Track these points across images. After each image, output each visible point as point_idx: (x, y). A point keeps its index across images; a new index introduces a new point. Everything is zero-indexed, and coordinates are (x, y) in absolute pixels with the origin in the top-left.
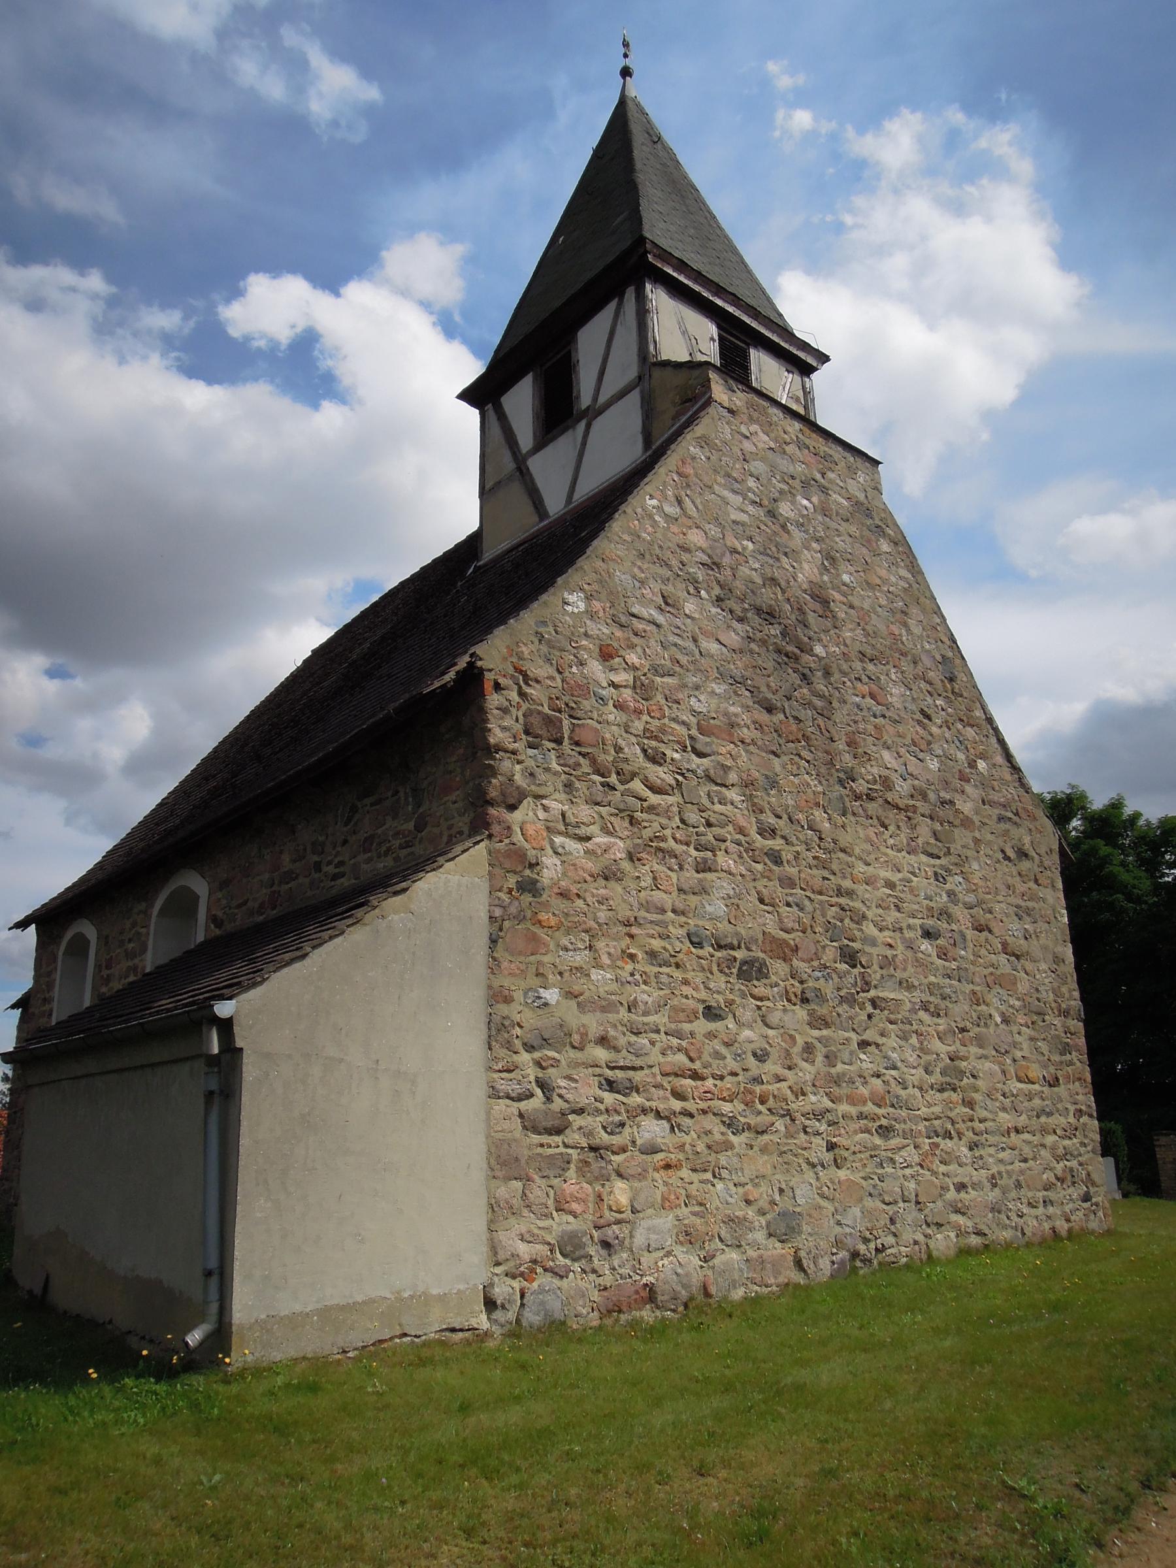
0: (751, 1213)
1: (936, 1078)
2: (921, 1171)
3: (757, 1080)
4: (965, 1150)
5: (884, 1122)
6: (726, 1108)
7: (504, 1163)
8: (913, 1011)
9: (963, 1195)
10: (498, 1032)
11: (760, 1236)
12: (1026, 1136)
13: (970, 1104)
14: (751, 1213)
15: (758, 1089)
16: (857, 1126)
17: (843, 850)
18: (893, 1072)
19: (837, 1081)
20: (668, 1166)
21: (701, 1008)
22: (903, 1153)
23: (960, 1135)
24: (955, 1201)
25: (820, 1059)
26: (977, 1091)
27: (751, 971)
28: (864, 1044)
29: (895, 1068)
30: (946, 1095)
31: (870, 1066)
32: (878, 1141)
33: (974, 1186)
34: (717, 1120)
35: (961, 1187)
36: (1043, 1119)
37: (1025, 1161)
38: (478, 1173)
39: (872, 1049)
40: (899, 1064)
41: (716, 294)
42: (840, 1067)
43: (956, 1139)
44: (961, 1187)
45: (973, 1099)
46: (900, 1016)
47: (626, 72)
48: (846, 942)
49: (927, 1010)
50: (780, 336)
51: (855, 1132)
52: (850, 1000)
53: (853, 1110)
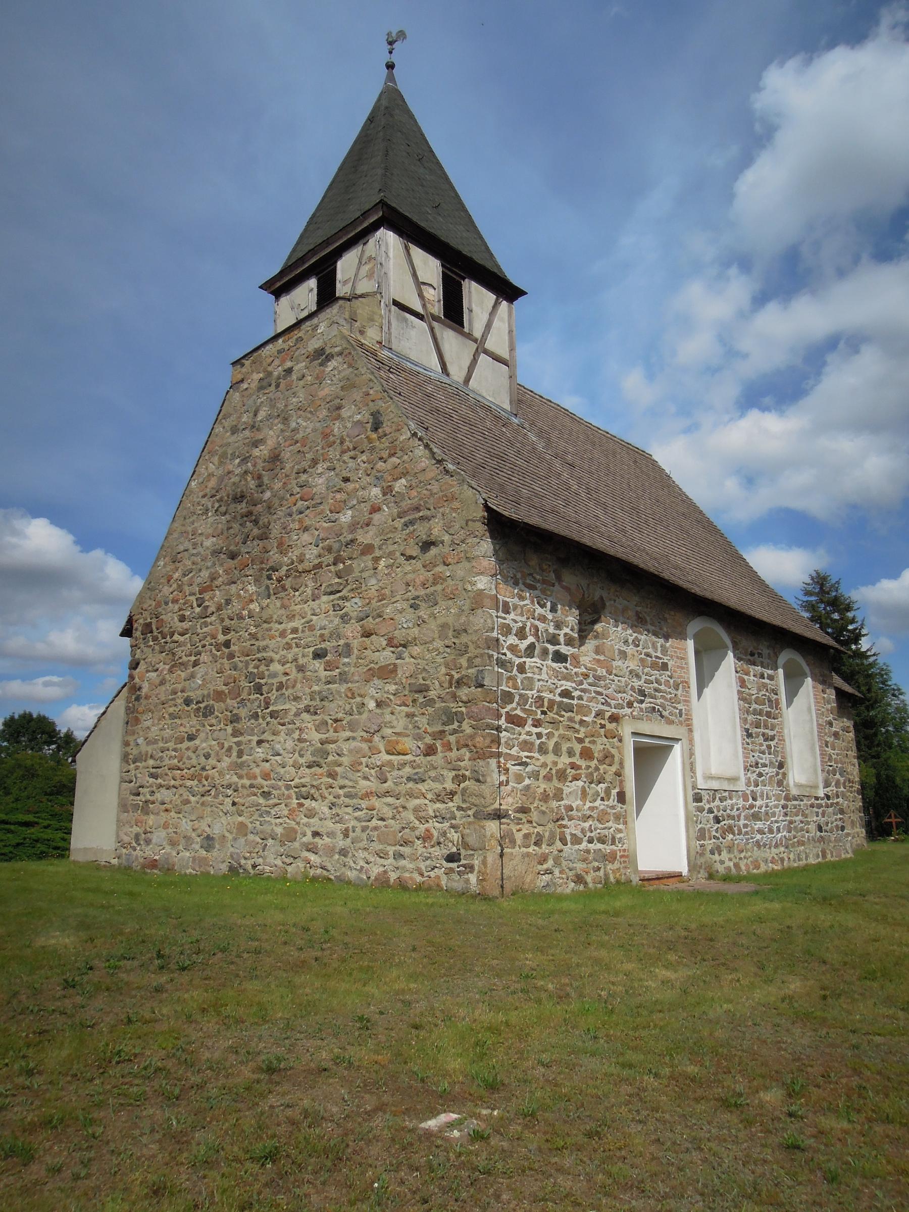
0: (194, 835)
1: (309, 757)
2: (288, 821)
3: (203, 769)
4: (326, 810)
5: (266, 789)
6: (189, 783)
7: (124, 807)
8: (297, 714)
9: (317, 839)
10: (125, 758)
11: (197, 847)
12: (389, 800)
13: (332, 775)
14: (194, 835)
15: (204, 773)
16: (249, 792)
17: (265, 622)
18: (277, 758)
19: (241, 766)
20: (167, 810)
21: (186, 735)
22: (276, 809)
23: (324, 798)
24: (310, 844)
25: (235, 754)
26: (340, 765)
27: (208, 712)
28: (260, 742)
29: (279, 755)
30: (313, 769)
31: (261, 755)
32: (261, 801)
33: (329, 835)
34: (185, 789)
35: (316, 834)
36: (411, 785)
37: (382, 819)
38: (115, 811)
39: (265, 745)
40: (282, 752)
41: (304, 263)
42: (245, 757)
43: (320, 801)
44: (316, 834)
45: (335, 771)
46: (287, 720)
47: (390, 66)
48: (257, 680)
49: (308, 712)
50: (345, 235)
51: (248, 796)
52: (256, 716)
53: (247, 782)
